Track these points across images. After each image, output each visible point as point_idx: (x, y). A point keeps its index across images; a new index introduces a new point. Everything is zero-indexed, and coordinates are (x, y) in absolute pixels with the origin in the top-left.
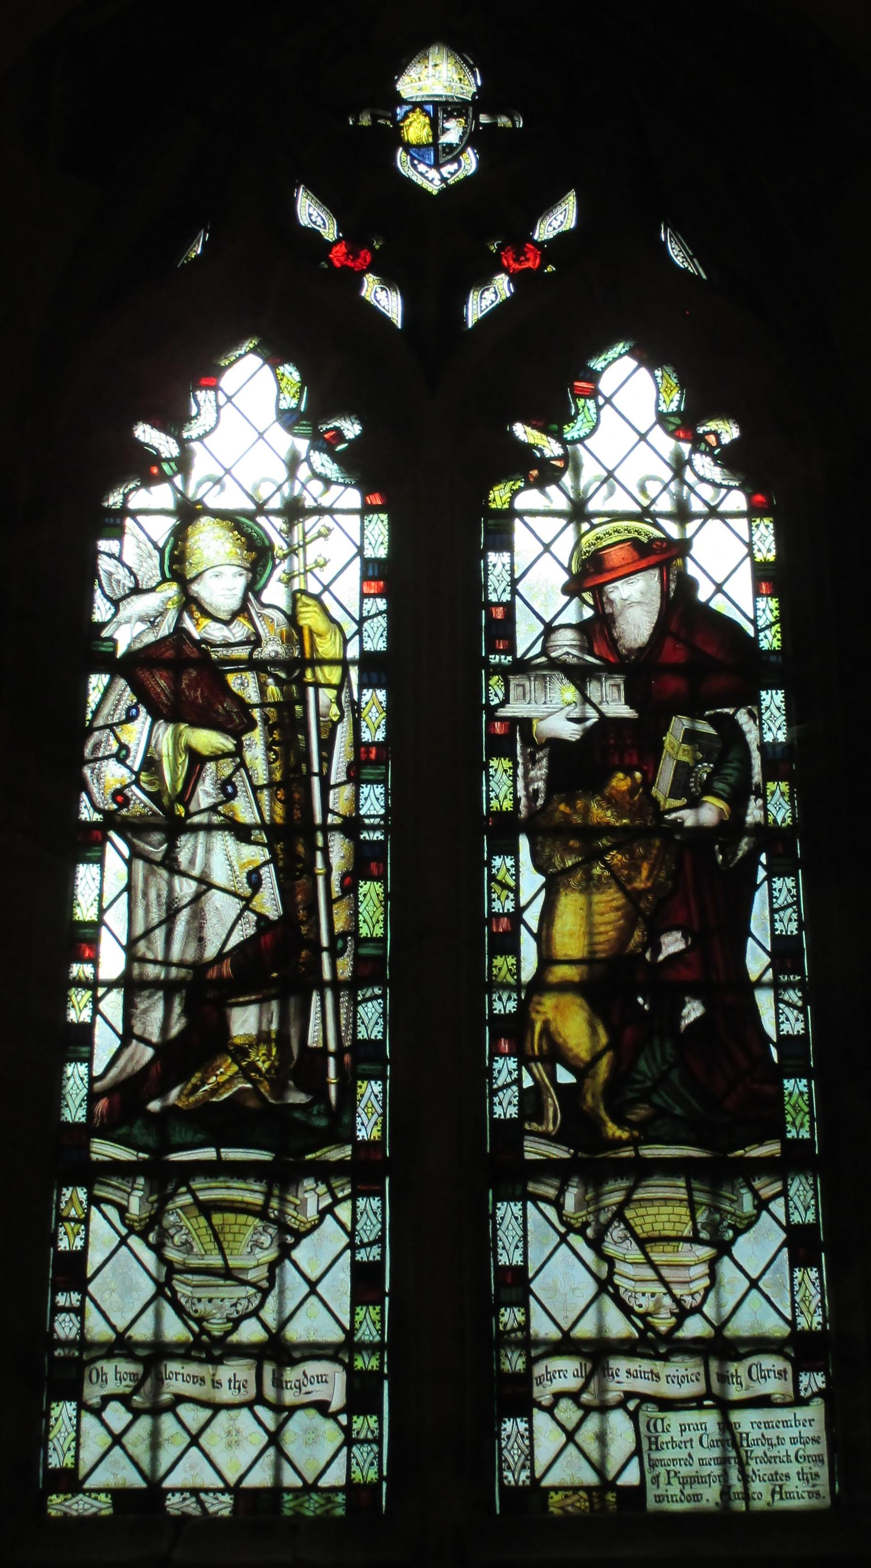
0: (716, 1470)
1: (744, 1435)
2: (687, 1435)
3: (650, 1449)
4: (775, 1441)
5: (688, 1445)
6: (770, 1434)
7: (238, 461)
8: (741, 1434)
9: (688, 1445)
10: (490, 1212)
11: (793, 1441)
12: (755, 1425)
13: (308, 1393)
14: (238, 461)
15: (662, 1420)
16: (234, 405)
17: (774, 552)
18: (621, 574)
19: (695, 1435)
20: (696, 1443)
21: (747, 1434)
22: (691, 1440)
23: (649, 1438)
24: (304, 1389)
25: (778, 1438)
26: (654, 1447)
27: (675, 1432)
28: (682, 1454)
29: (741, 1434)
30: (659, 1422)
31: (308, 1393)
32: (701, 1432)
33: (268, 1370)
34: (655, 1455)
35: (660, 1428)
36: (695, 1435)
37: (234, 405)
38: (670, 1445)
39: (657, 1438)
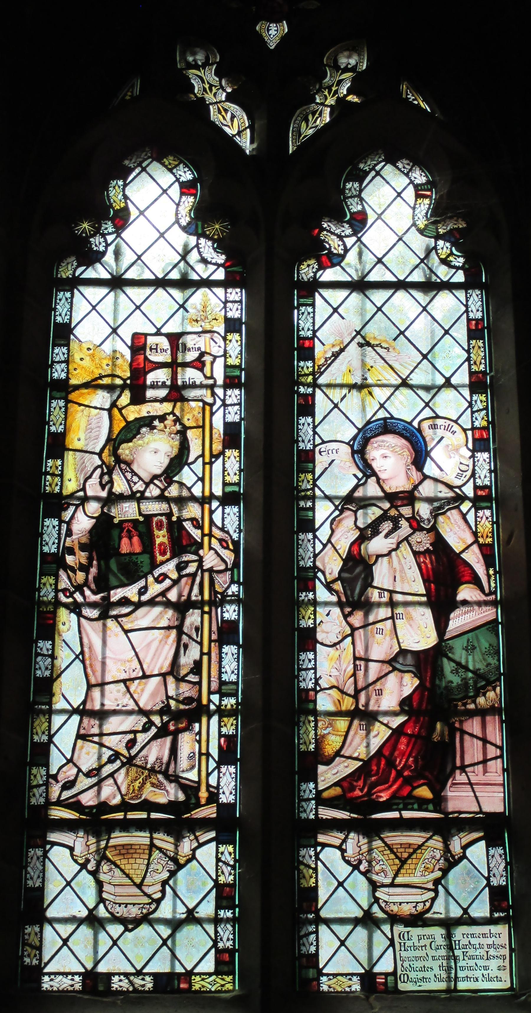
0: (461, 974)
1: (457, 942)
2: (422, 943)
3: (401, 950)
4: (478, 946)
5: (424, 948)
6: (473, 941)
7: (156, 200)
8: (455, 941)
9: (424, 948)
10: (20, 954)
11: (489, 946)
12: (465, 936)
13: (420, 986)
14: (156, 200)
15: (408, 932)
16: (148, 207)
17: (310, 262)
18: (212, 666)
19: (427, 942)
20: (428, 947)
21: (459, 941)
22: (425, 946)
23: (400, 943)
24: (418, 984)
25: (479, 944)
26: (403, 949)
27: (415, 939)
28: (418, 953)
29: (455, 941)
30: (406, 934)
31: (420, 986)
32: (431, 940)
33: (453, 987)
34: (404, 954)
35: (406, 938)
36: (427, 942)
37: (148, 207)
38: (412, 948)
39: (404, 943)
